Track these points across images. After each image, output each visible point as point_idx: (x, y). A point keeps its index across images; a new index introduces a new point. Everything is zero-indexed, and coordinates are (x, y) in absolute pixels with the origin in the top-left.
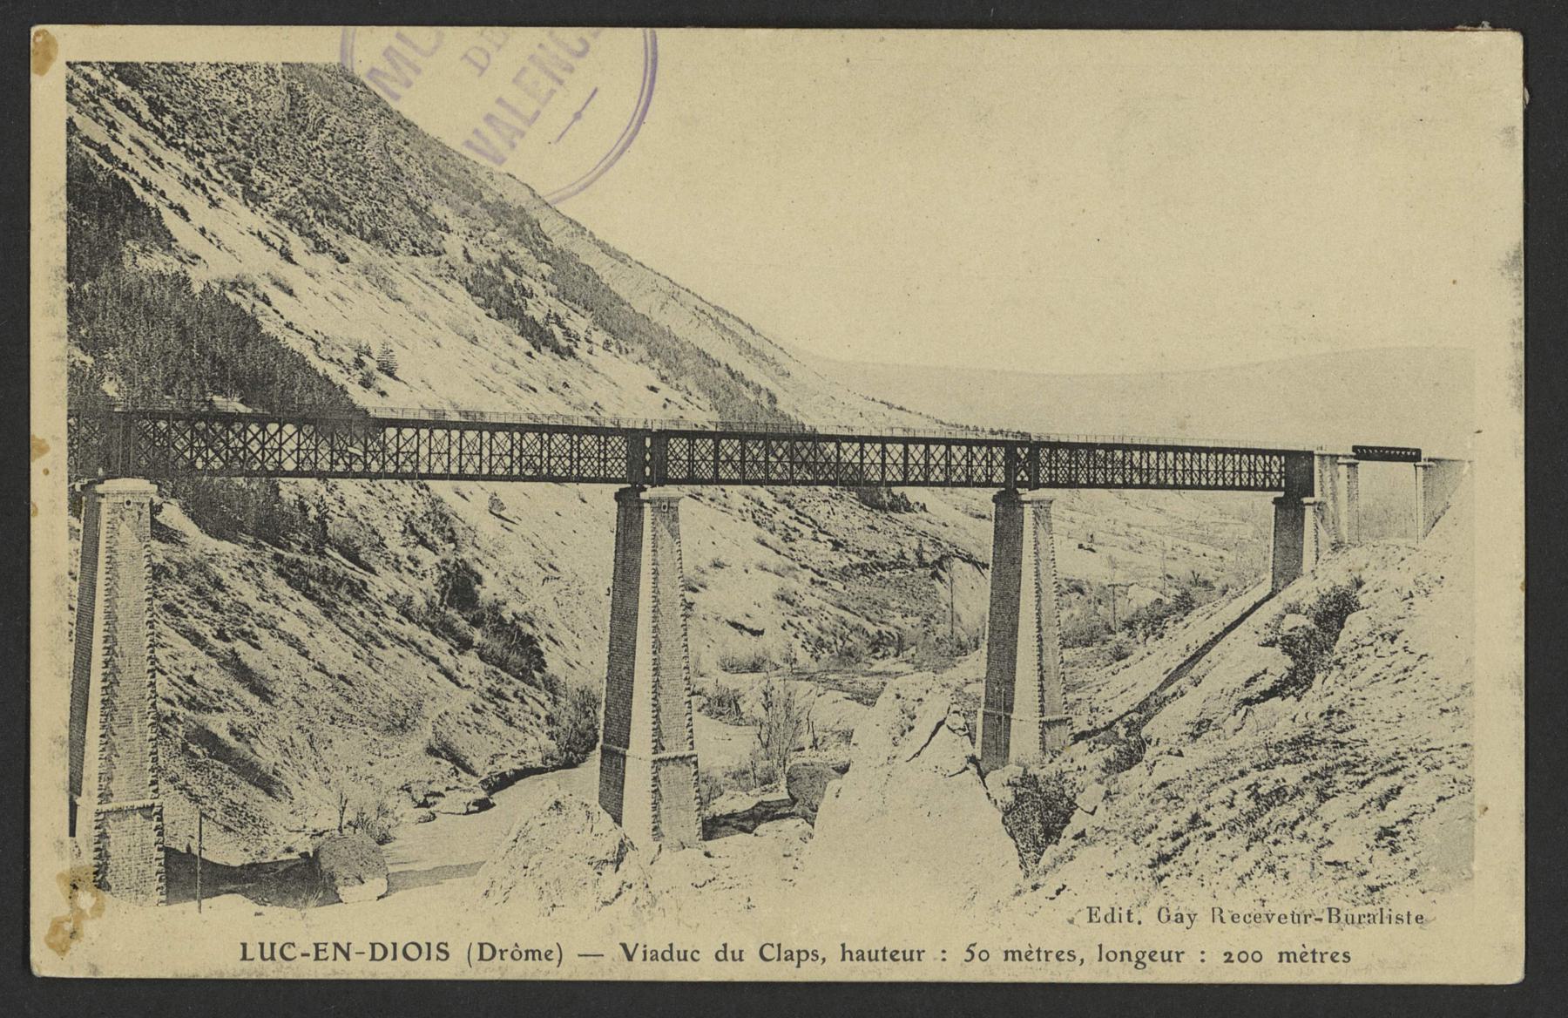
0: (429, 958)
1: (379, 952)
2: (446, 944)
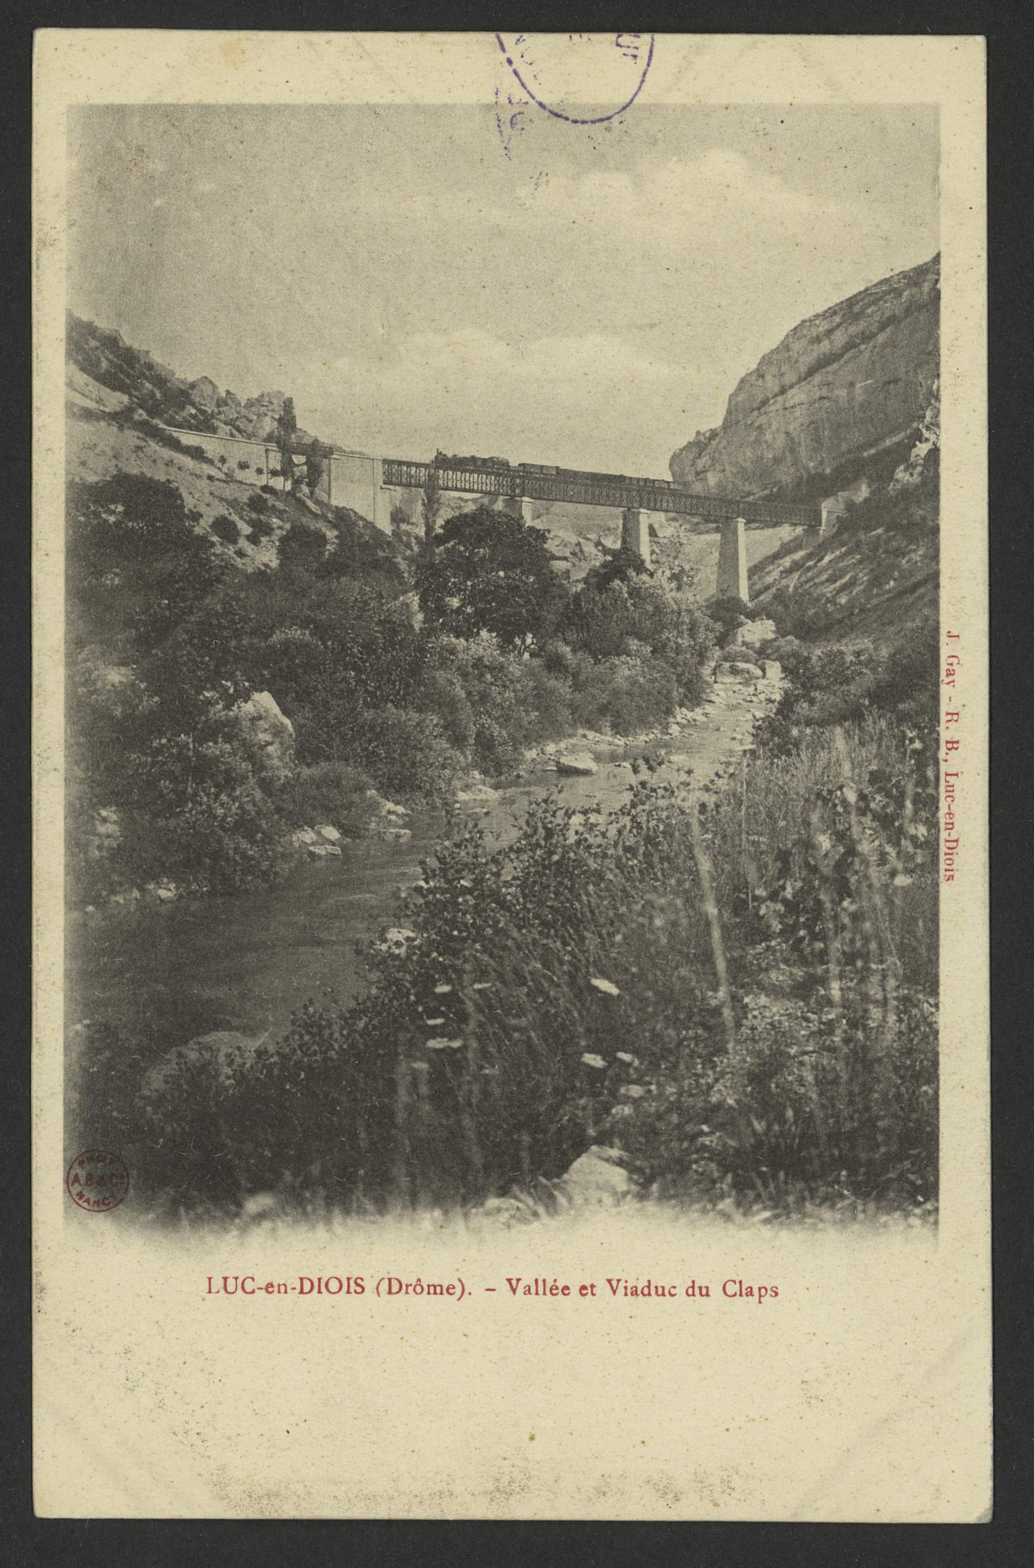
0: (348, 1292)
1: (307, 1286)
2: (362, 1279)
